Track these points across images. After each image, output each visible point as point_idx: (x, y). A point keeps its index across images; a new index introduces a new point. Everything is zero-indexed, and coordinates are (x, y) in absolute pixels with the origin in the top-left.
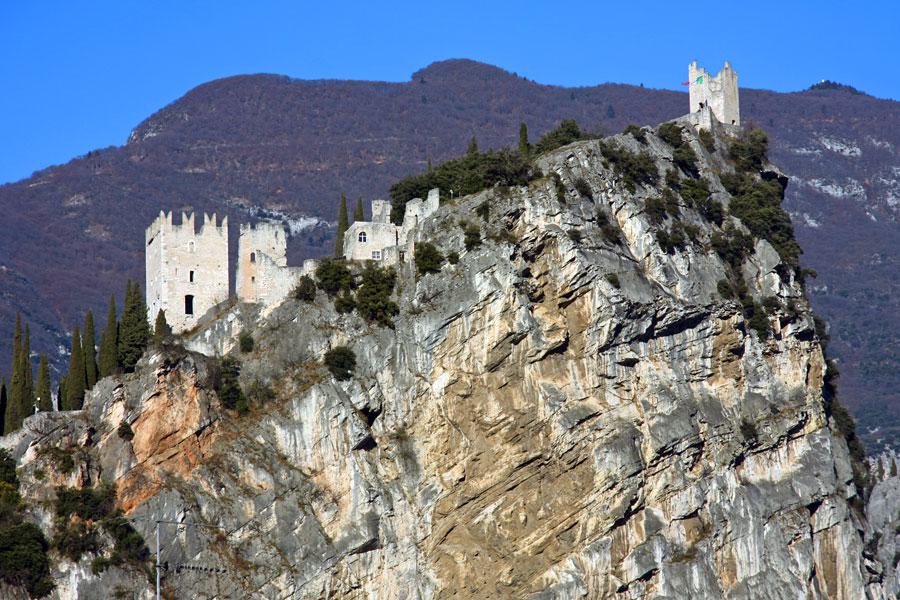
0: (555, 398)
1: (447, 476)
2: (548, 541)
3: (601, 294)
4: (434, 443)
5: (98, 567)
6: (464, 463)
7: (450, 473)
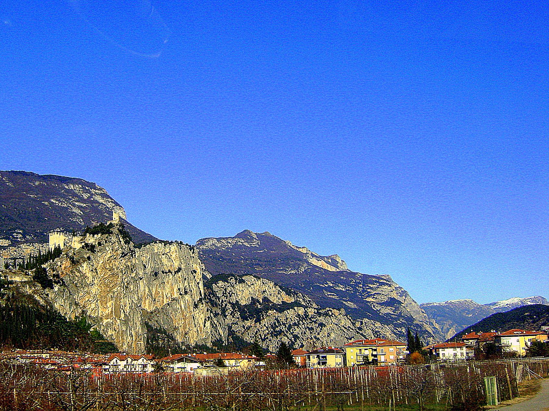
5: (60, 286)
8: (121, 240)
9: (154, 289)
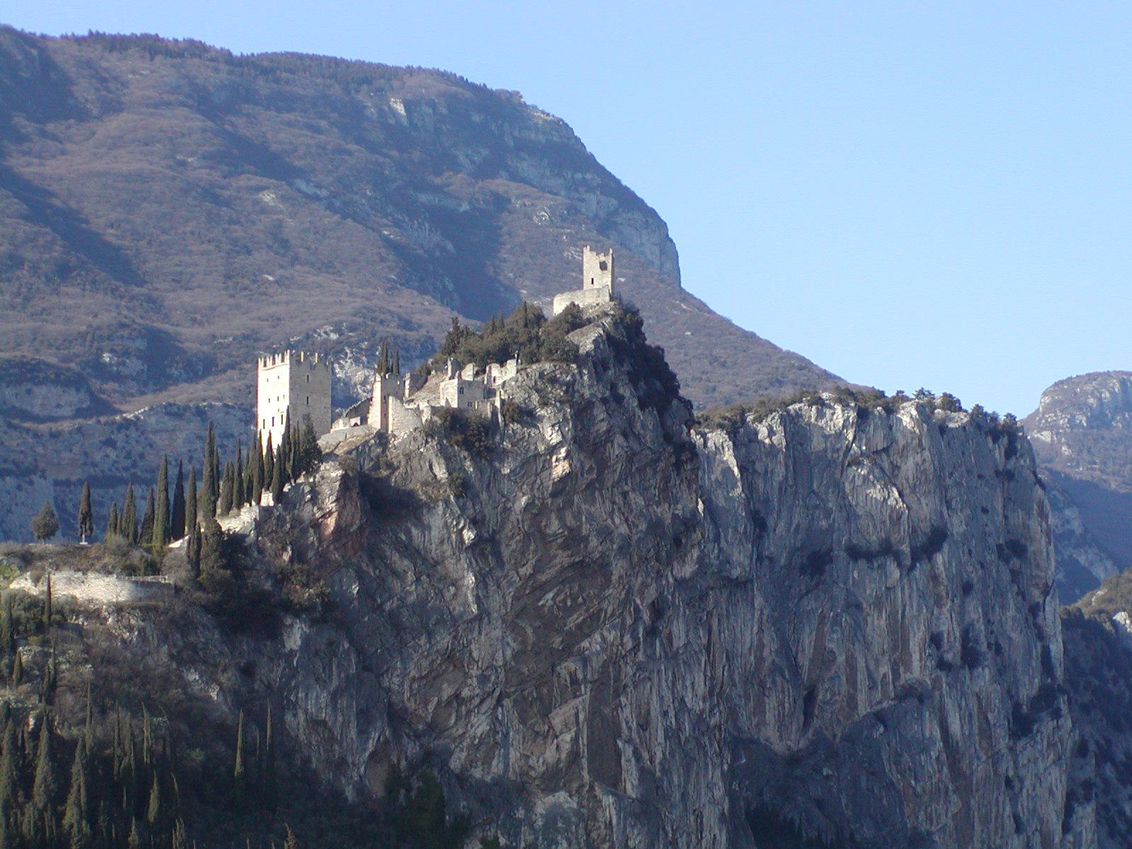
0: (591, 517)
1: (522, 571)
2: (584, 621)
3: (619, 446)
4: (514, 546)
6: (533, 561)
7: (525, 568)
8: (625, 391)
9: (808, 639)
